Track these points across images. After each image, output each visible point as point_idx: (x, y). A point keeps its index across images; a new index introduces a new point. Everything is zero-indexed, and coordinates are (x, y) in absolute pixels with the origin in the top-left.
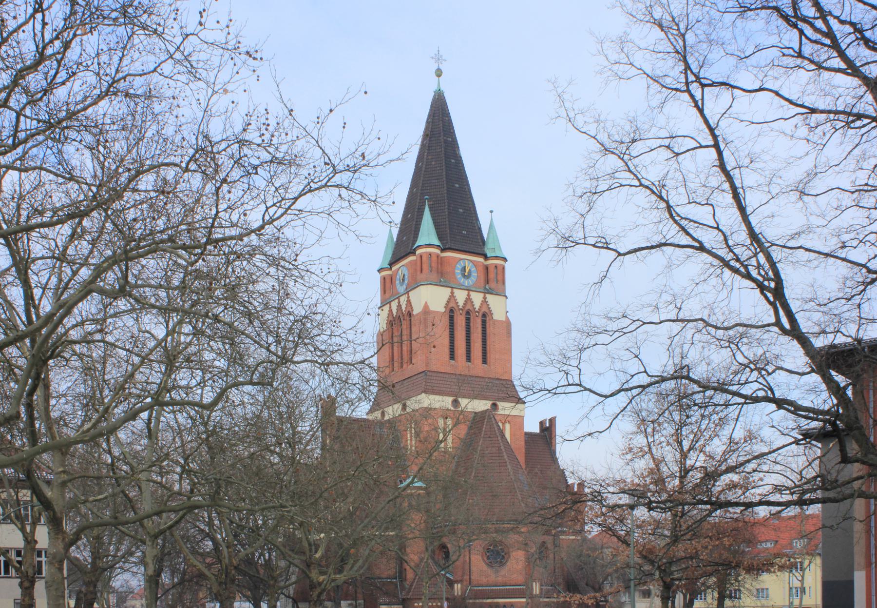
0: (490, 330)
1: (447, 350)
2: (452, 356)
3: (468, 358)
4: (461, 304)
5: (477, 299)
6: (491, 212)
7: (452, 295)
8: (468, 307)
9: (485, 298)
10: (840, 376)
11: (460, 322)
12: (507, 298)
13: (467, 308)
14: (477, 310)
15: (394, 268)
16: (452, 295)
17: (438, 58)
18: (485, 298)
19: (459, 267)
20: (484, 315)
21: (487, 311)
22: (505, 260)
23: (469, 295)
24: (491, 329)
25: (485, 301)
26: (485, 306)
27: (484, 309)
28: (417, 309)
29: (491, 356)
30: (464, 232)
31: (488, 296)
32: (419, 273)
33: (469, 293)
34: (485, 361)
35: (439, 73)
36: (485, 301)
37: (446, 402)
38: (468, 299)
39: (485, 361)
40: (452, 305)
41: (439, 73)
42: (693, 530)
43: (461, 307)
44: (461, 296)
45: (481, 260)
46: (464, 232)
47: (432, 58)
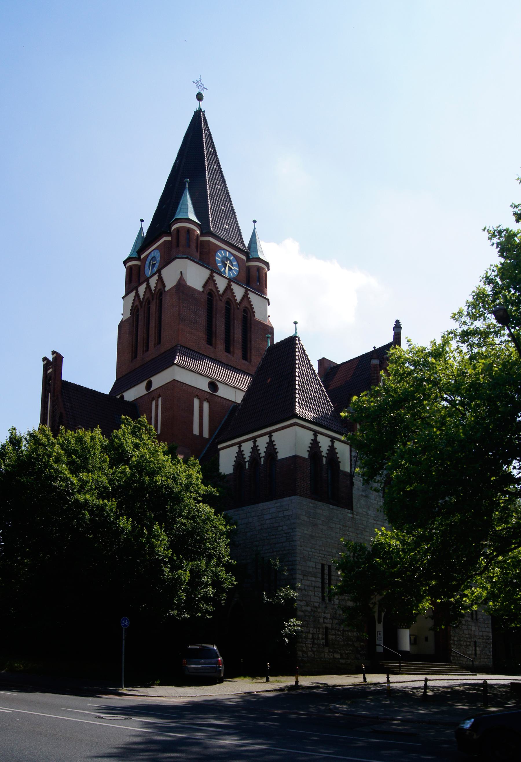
5: (239, 292)
6: (255, 221)
7: (211, 279)
12: (269, 305)
15: (142, 257)
17: (199, 84)
22: (267, 264)
25: (245, 297)
27: (245, 304)
28: (170, 283)
35: (200, 97)
38: (228, 288)
41: (200, 97)
45: (244, 258)
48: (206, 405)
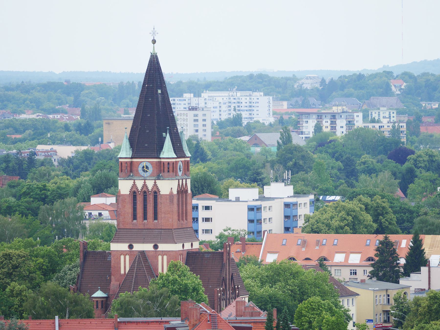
0: (159, 200)
1: (130, 216)
2: (135, 217)
3: (145, 217)
4: (140, 188)
5: (150, 184)
7: (134, 184)
8: (145, 189)
9: (155, 183)
10: (337, 197)
11: (140, 199)
13: (153, 190)
14: (150, 190)
16: (134, 184)
18: (155, 183)
19: (141, 166)
20: (155, 192)
21: (157, 190)
23: (145, 182)
24: (159, 200)
25: (155, 184)
26: (155, 187)
27: (155, 189)
29: (159, 216)
30: (146, 145)
31: (157, 181)
32: (120, 172)
33: (145, 181)
34: (156, 218)
35: (154, 42)
36: (155, 184)
37: (124, 247)
38: (145, 185)
39: (156, 218)
40: (134, 189)
41: (154, 42)
42: (148, 289)
43: (140, 190)
44: (140, 184)
46: (146, 145)
47: (150, 33)
48: (127, 257)
